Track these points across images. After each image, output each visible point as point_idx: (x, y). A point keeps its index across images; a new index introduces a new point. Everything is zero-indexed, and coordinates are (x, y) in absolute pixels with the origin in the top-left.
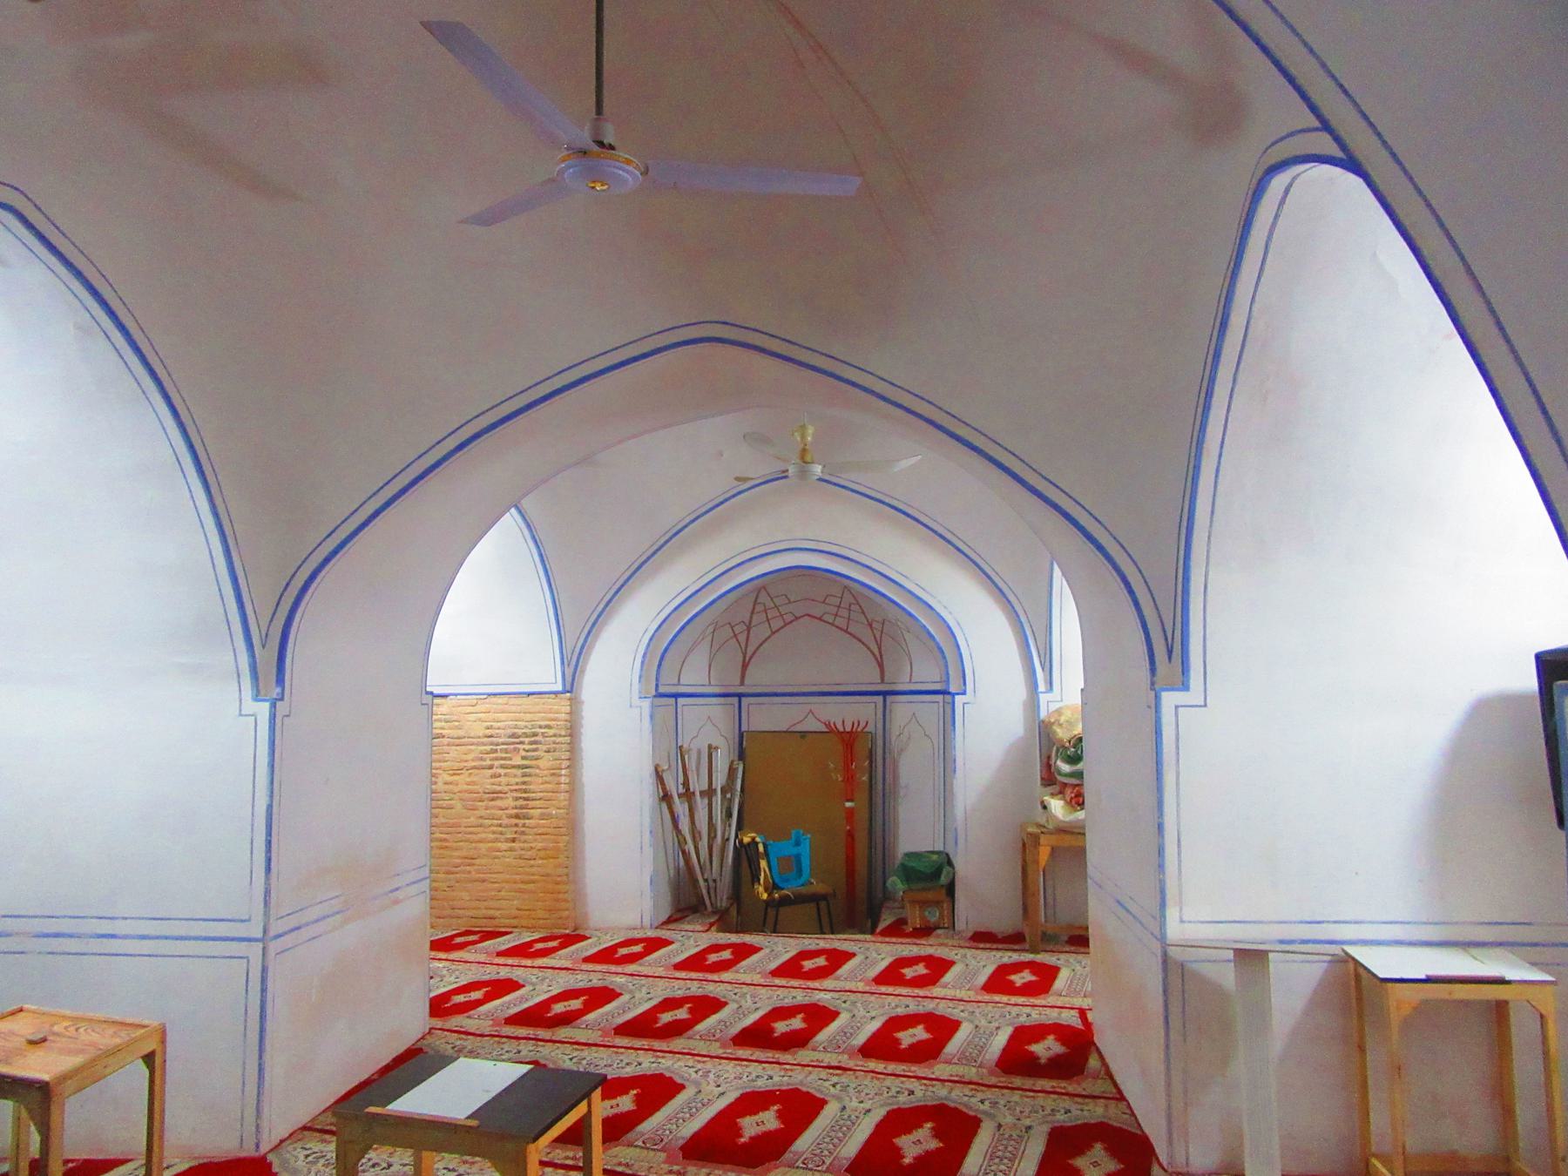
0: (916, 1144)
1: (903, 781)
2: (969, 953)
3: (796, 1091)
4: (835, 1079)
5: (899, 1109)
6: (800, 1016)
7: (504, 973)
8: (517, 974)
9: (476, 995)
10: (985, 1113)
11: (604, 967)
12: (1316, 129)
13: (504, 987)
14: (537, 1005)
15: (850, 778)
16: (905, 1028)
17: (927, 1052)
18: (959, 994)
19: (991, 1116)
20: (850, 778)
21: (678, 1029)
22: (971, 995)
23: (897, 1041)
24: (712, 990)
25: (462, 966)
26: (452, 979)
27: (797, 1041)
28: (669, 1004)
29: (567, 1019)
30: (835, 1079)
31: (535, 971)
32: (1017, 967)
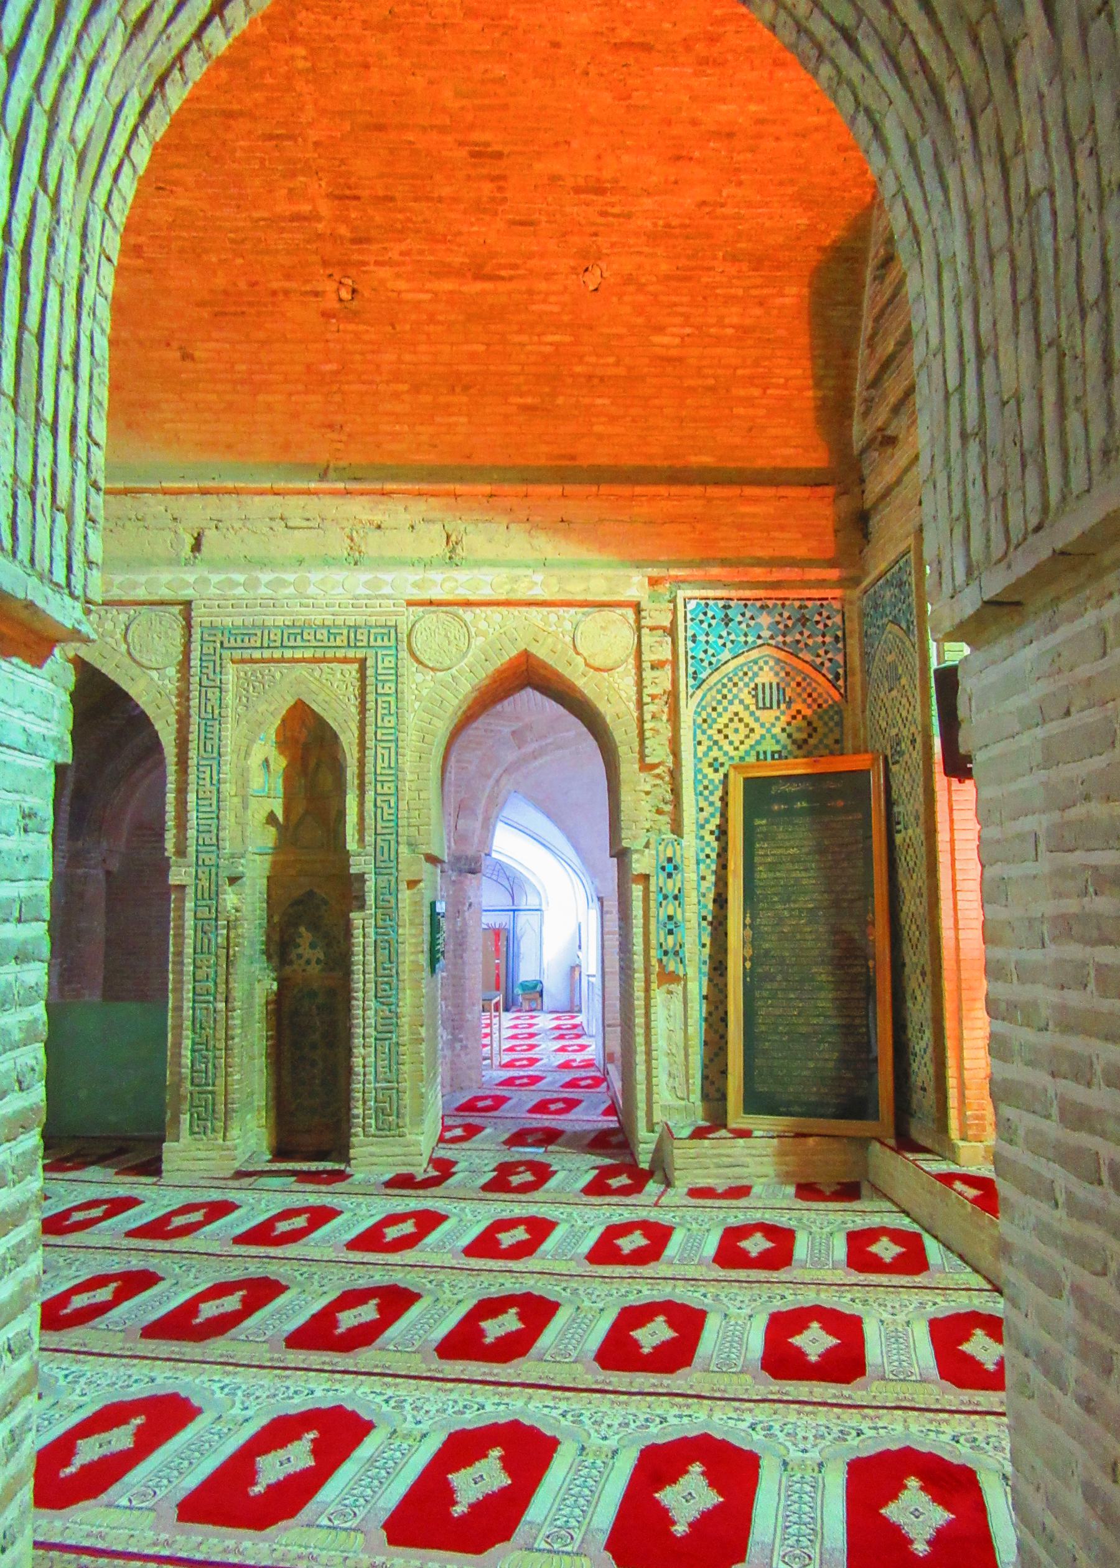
0: (689, 1498)
1: (522, 950)
2: (690, 1213)
3: (340, 1408)
4: (563, 1406)
5: (463, 1432)
6: (513, 1311)
7: (136, 1263)
8: (154, 1263)
9: (104, 1294)
10: (384, 1415)
11: (261, 1250)
12: (182, 69)
13: (136, 1282)
14: (314, 1317)
15: (497, 950)
16: (641, 1324)
17: (676, 1356)
18: (560, 1267)
19: (572, 1436)
20: (497, 950)
21: (365, 1335)
22: (573, 1268)
23: (636, 1345)
24: (272, 1271)
25: (82, 1255)
26: (72, 1272)
27: (512, 1348)
28: (351, 1299)
29: (223, 1324)
30: (563, 1406)
31: (64, 1251)
32: (625, 1229)
